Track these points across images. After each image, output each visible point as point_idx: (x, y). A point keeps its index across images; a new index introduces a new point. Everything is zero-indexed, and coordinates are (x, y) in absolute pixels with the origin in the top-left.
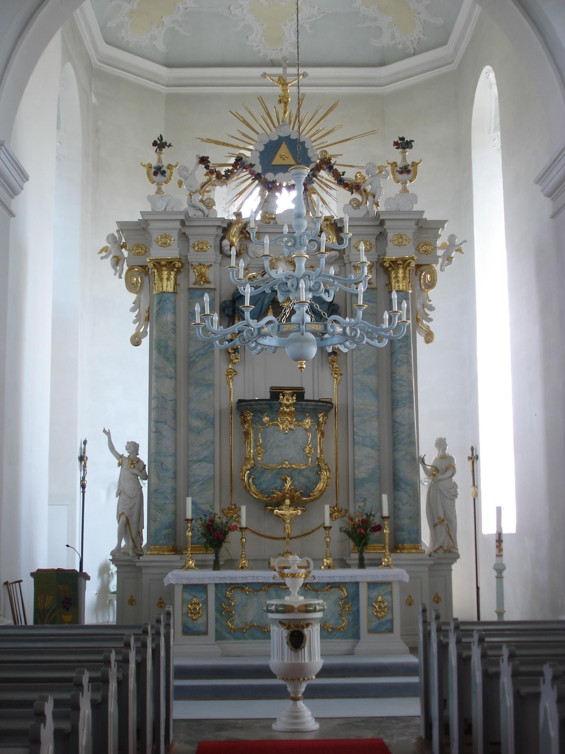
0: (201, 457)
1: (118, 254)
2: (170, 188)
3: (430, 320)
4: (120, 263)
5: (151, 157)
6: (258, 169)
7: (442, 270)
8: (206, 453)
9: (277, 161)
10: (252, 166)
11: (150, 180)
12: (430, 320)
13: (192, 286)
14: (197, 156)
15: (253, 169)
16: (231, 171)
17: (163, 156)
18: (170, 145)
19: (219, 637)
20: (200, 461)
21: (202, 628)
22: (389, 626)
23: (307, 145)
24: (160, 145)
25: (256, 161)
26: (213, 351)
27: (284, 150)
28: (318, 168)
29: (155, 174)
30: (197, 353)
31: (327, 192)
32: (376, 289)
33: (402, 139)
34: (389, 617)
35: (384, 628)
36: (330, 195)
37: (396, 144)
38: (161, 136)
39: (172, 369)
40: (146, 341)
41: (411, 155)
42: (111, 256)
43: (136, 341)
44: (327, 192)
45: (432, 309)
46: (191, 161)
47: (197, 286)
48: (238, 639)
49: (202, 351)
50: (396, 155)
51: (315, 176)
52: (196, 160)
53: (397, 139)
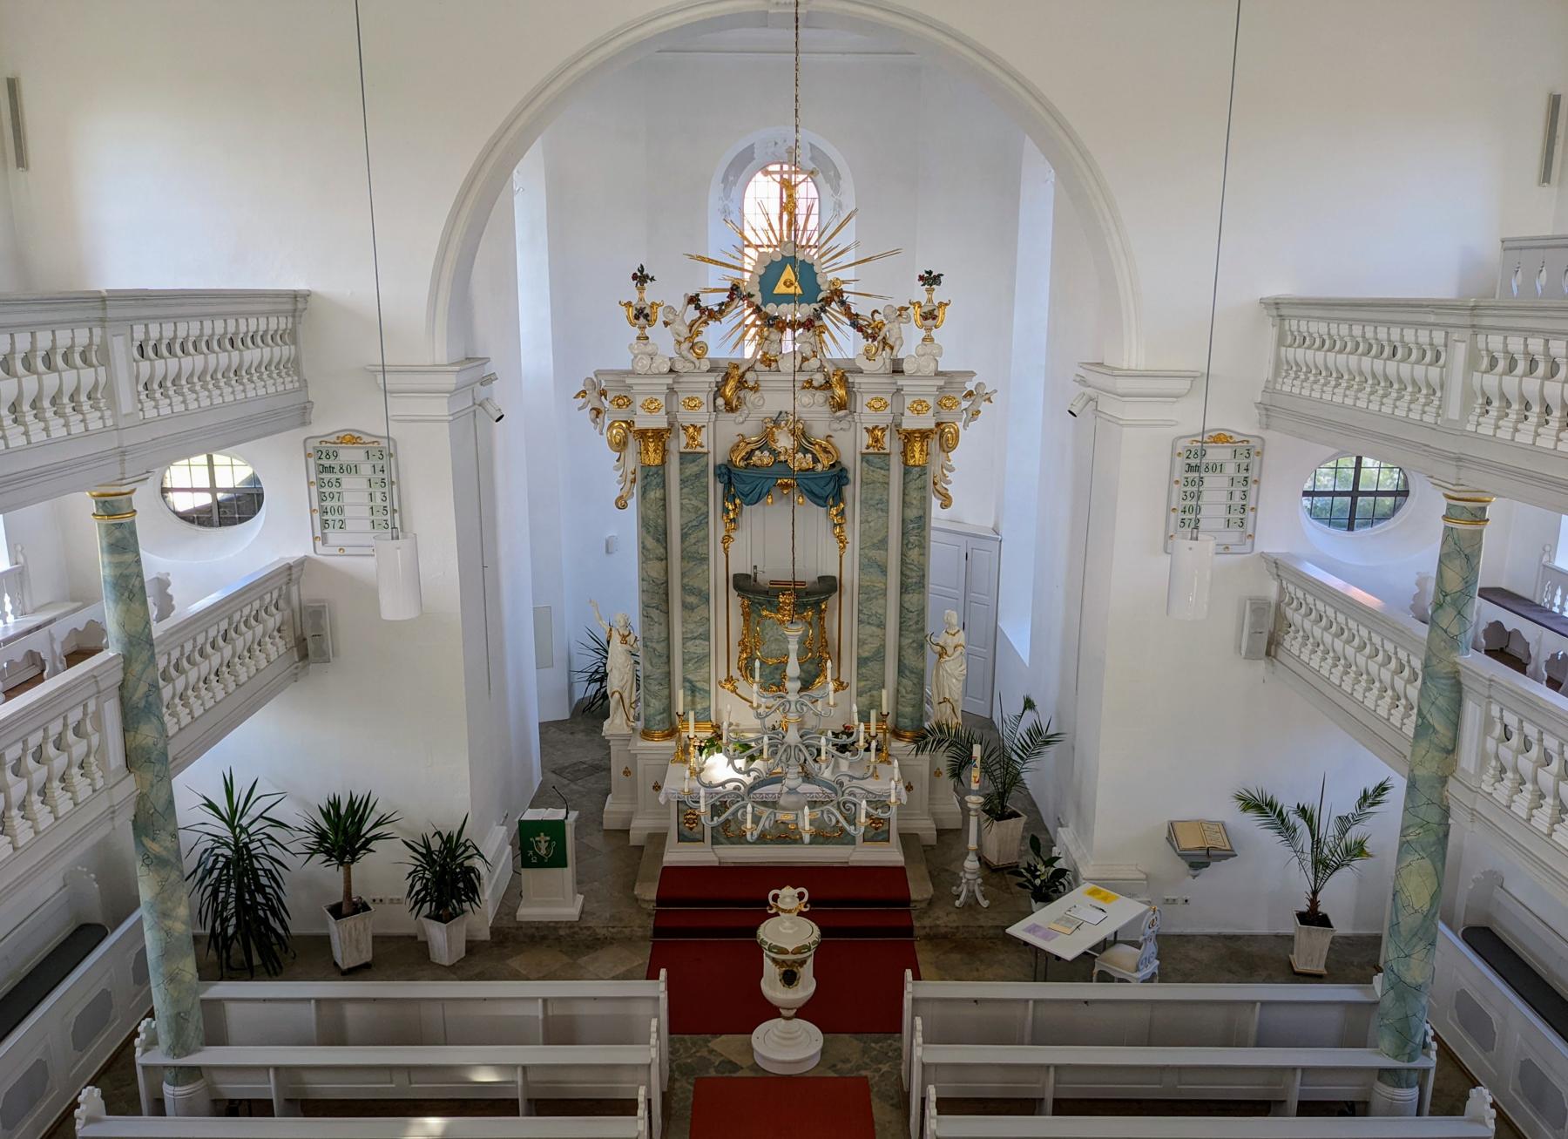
0: (695, 635)
1: (597, 405)
2: (656, 332)
3: (949, 482)
4: (601, 416)
5: (631, 293)
6: (758, 299)
7: (965, 427)
8: (701, 630)
9: (780, 289)
10: (750, 295)
11: (631, 323)
12: (949, 482)
13: (682, 450)
14: (686, 295)
15: (752, 299)
16: (727, 305)
17: (645, 295)
18: (652, 279)
19: (715, 841)
20: (695, 638)
21: (699, 836)
22: (885, 835)
23: (816, 269)
24: (641, 278)
25: (755, 290)
26: (707, 522)
27: (788, 274)
28: (827, 301)
29: (637, 317)
30: (690, 525)
31: (838, 327)
32: (888, 454)
33: (930, 273)
34: (886, 828)
35: (881, 838)
36: (842, 331)
37: (921, 278)
38: (642, 266)
39: (662, 550)
40: (633, 503)
41: (939, 294)
42: (590, 407)
43: (621, 504)
44: (838, 327)
45: (951, 470)
46: (679, 303)
47: (688, 450)
48: (734, 844)
49: (695, 523)
50: (920, 293)
51: (825, 311)
52: (683, 301)
53: (923, 273)
